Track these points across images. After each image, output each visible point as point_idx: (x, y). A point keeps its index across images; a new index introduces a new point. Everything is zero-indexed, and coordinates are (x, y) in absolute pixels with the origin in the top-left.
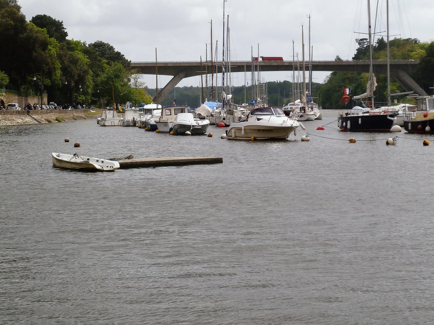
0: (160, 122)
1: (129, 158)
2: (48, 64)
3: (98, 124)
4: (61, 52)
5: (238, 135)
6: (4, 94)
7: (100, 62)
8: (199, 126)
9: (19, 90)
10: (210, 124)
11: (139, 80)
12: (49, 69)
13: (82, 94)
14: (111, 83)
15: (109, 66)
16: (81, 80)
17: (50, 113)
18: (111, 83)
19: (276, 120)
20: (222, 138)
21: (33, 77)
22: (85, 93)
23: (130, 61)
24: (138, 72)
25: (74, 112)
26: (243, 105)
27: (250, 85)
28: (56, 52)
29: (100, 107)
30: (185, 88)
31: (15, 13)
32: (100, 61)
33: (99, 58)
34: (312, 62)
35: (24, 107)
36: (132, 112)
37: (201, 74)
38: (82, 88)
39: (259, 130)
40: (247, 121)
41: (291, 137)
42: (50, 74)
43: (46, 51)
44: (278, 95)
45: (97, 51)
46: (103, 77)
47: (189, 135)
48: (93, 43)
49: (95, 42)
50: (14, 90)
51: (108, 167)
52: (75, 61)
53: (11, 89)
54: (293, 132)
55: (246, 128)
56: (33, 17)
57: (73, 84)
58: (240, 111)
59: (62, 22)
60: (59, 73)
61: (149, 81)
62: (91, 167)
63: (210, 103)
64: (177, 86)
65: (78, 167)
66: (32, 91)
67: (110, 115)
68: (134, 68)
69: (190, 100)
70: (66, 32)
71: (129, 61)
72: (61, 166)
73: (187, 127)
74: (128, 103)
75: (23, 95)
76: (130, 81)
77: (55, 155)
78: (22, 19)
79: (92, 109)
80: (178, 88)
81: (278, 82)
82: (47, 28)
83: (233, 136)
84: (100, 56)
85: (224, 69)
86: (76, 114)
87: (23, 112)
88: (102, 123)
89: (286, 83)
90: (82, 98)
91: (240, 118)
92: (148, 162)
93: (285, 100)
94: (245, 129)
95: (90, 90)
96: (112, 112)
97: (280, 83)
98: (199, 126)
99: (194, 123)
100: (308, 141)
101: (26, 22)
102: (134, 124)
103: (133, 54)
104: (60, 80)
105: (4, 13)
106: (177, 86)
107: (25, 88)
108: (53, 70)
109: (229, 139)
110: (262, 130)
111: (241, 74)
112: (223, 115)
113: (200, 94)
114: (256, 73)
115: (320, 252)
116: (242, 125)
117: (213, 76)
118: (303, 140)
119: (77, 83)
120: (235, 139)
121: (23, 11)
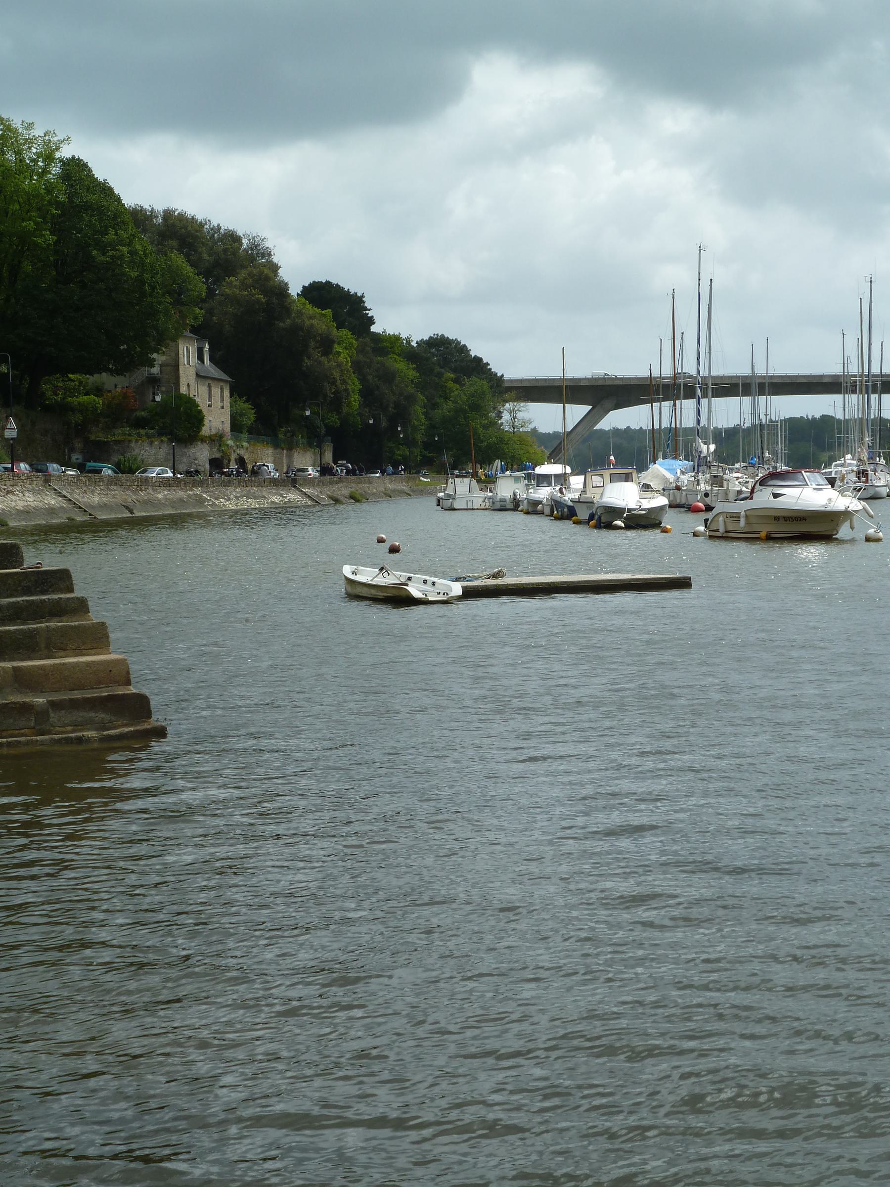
0: (579, 502)
1: (495, 576)
2: (334, 383)
3: (438, 505)
4: (361, 357)
5: (731, 527)
6: (245, 444)
7: (440, 378)
8: (642, 510)
9: (276, 435)
10: (671, 506)
11: (520, 415)
12: (336, 393)
13: (402, 445)
14: (463, 421)
15: (458, 386)
16: (401, 415)
17: (337, 483)
18: (463, 421)
19: (810, 494)
20: (696, 534)
21: (304, 410)
22: (409, 442)
23: (503, 376)
24: (519, 399)
25: (387, 481)
26: (737, 465)
27: (748, 424)
28: (351, 357)
29: (439, 472)
30: (616, 432)
31: (267, 279)
32: (440, 375)
33: (437, 369)
34: (882, 375)
35: (285, 470)
36: (511, 481)
37: (651, 401)
38: (403, 431)
39: (777, 519)
40: (752, 498)
41: (844, 532)
42: (337, 403)
43: (331, 356)
44: (810, 446)
45: (433, 355)
46: (446, 409)
47: (620, 528)
48: (426, 338)
49: (431, 337)
50: (265, 435)
51: (439, 593)
52: (389, 377)
53: (259, 433)
54: (847, 524)
55: (748, 513)
56: (304, 287)
57: (384, 424)
58: (737, 479)
59: (363, 296)
60: (355, 400)
61: (546, 418)
62: (403, 594)
63: (669, 461)
64: (597, 427)
65: (381, 594)
66: (302, 437)
67: (462, 488)
68: (509, 389)
69: (632, 453)
70: (372, 317)
71: (499, 375)
72: (358, 593)
73: (616, 511)
74: (498, 463)
75: (283, 445)
76: (501, 417)
77: (347, 570)
78: (282, 289)
79: (424, 476)
80: (601, 431)
81: (810, 417)
82: (333, 310)
83: (722, 530)
84: (439, 365)
85: (699, 391)
86: (390, 485)
87: (284, 481)
88: (447, 504)
89: (826, 420)
90: (403, 451)
91: (740, 492)
92: (533, 584)
93: (825, 456)
94: (746, 516)
95: (419, 437)
96: (467, 480)
97: (814, 419)
98: (642, 510)
99: (632, 505)
100: (878, 540)
101: (289, 295)
102: (515, 505)
103: (510, 361)
104: (360, 414)
105: (245, 279)
106: (598, 427)
107: (288, 431)
108: (345, 394)
109: (711, 537)
110: (784, 517)
111: (732, 402)
112: (703, 487)
113: (649, 443)
114: (762, 399)
115: (417, 770)
116: (741, 507)
117: (675, 405)
118: (868, 539)
119: (393, 423)
120: (727, 537)
121: (284, 274)
